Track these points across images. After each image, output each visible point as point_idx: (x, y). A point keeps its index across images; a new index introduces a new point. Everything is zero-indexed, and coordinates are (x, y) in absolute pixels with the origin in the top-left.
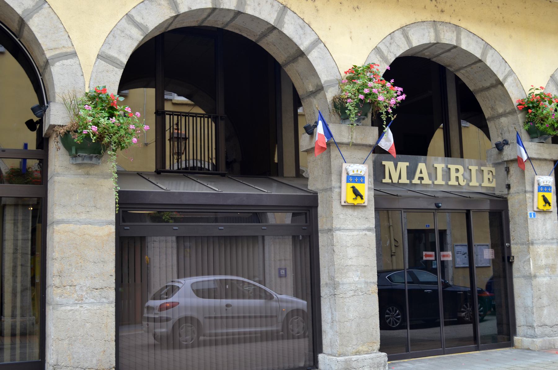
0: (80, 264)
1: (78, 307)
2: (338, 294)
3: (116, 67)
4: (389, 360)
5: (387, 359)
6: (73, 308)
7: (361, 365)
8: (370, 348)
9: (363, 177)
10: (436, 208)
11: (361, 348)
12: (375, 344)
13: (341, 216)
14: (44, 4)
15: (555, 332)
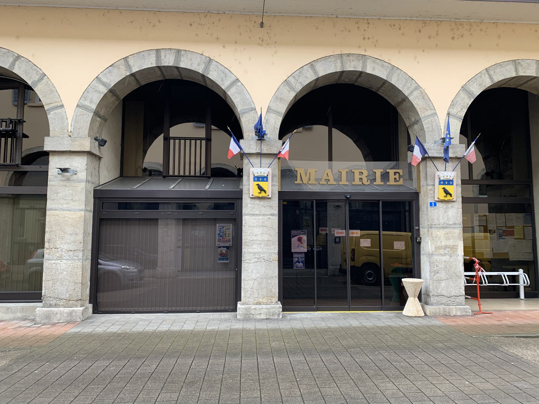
0: (62, 235)
1: (59, 261)
2: (244, 260)
3: (89, 112)
4: (283, 311)
5: (281, 310)
6: (56, 262)
7: (259, 313)
8: (269, 301)
9: (452, 181)
10: (345, 199)
11: (261, 300)
12: (274, 298)
13: (249, 205)
14: (44, 76)
15: (453, 302)
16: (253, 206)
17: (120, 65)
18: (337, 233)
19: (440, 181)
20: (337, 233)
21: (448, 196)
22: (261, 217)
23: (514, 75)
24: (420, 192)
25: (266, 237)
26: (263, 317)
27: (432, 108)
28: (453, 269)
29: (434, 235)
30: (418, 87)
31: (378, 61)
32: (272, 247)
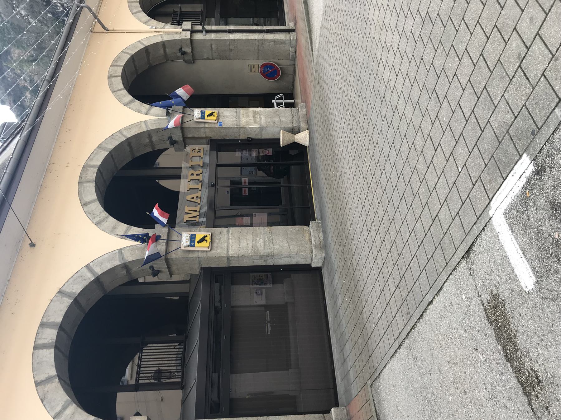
9: (191, 235)
13: (218, 251)
16: (219, 248)
17: (44, 391)
18: (245, 193)
19: (201, 118)
20: (245, 193)
21: (206, 238)
22: (230, 241)
23: (120, 78)
24: (210, 137)
25: (250, 237)
26: (321, 235)
27: (140, 123)
28: (271, 114)
29: (245, 124)
30: (120, 132)
31: (91, 157)
32: (258, 231)
